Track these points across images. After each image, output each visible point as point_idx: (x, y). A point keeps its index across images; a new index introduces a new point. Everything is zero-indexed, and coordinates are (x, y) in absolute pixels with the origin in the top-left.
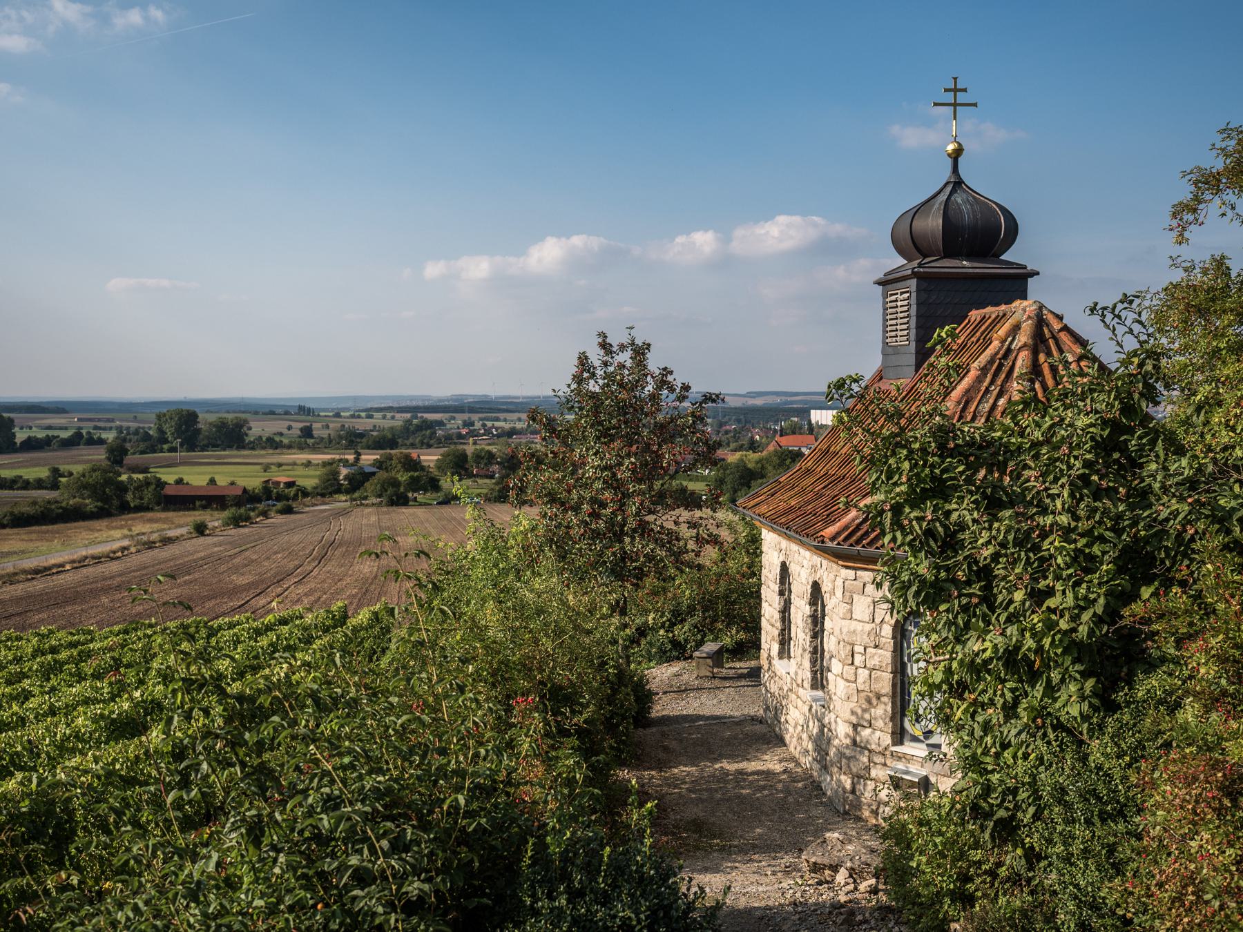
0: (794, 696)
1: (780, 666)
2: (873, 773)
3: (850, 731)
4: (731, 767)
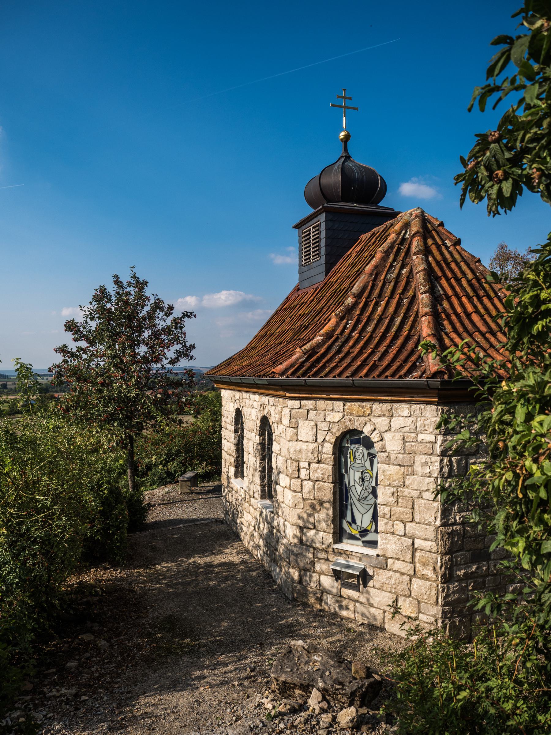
0: (247, 505)
1: (236, 483)
2: (318, 567)
3: (297, 532)
4: (201, 560)
